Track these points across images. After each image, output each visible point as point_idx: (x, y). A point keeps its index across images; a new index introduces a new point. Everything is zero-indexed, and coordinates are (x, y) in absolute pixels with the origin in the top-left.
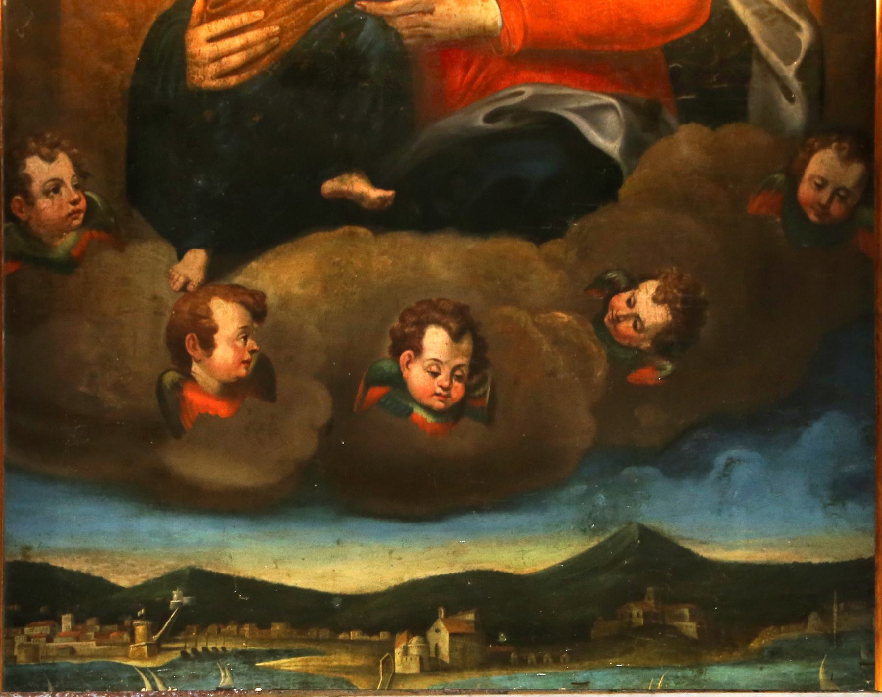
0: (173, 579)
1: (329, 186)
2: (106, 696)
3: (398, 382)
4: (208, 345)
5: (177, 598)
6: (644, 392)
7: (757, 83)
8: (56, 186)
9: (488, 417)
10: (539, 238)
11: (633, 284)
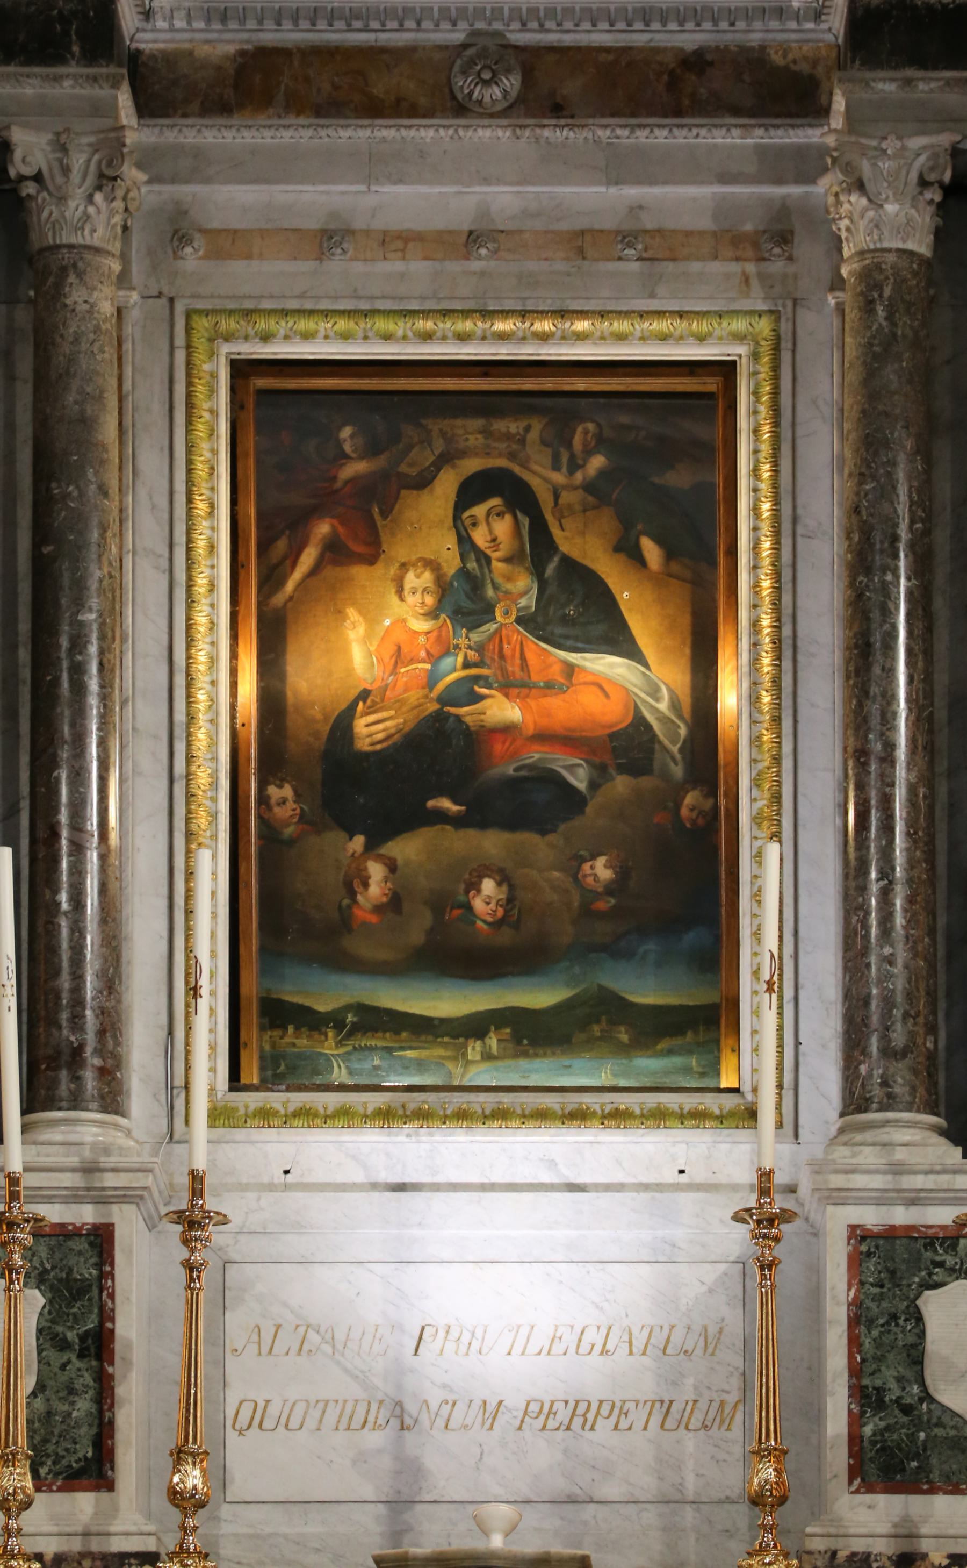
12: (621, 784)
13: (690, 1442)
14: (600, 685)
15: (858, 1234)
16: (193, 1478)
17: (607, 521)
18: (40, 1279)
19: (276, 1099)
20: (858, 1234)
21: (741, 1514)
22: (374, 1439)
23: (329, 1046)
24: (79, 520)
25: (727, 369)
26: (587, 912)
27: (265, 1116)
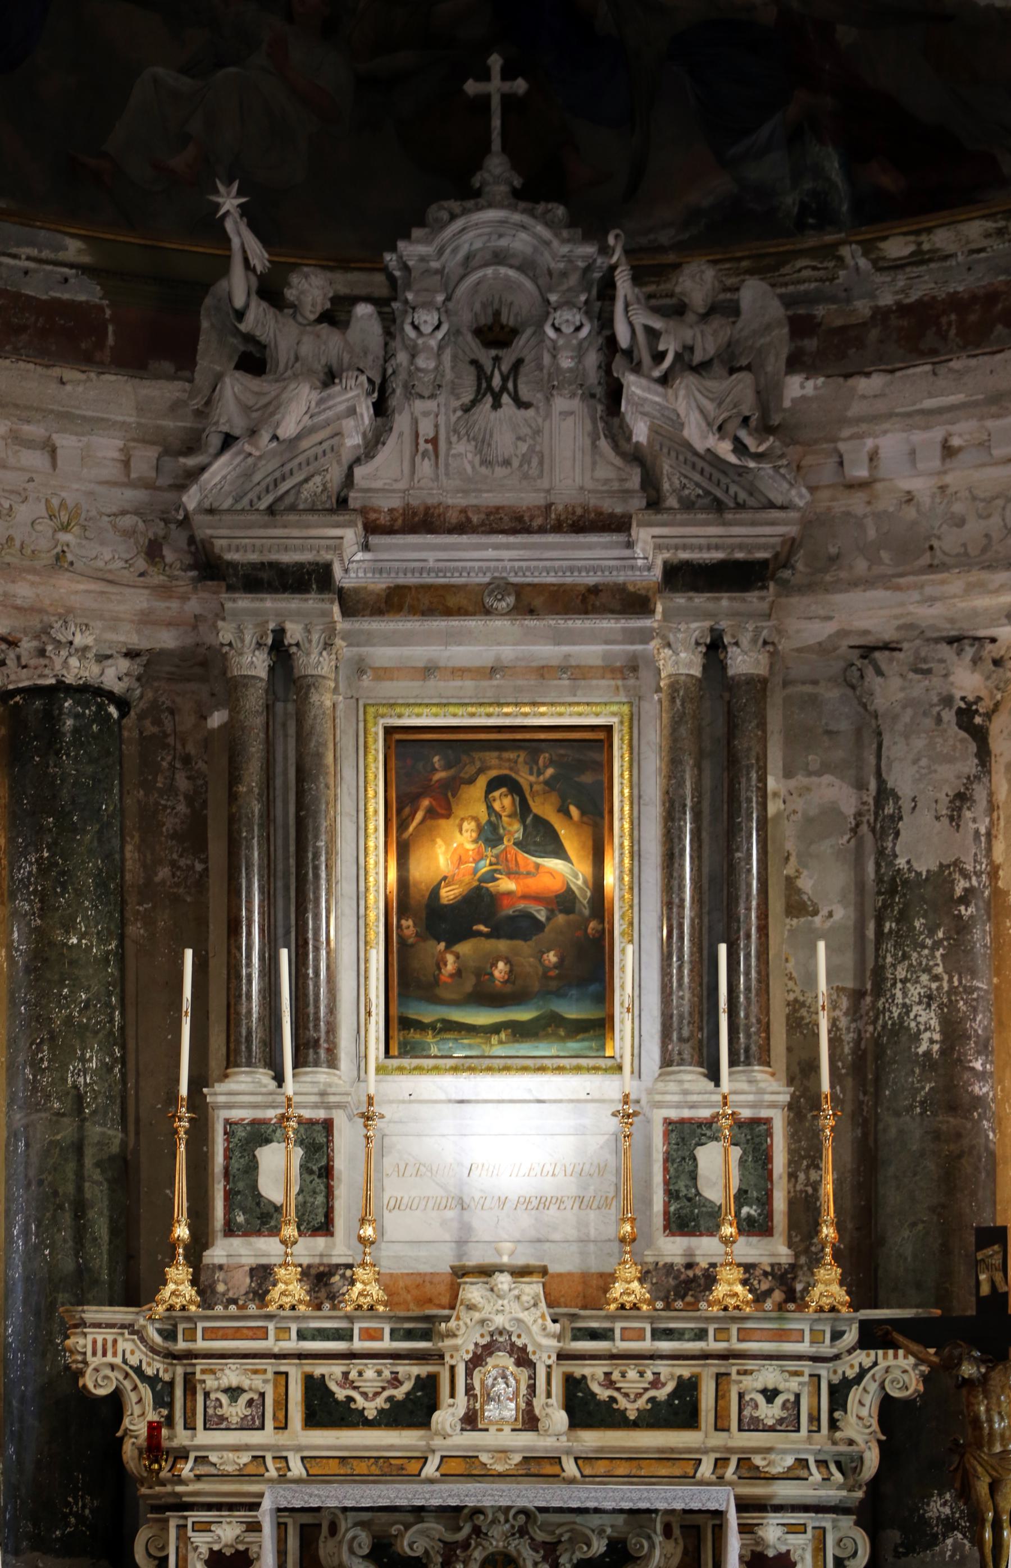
0: (438, 1021)
1: (475, 928)
2: (994, 1357)
3: (492, 975)
4: (446, 965)
5: (439, 1025)
6: (552, 978)
7: (577, 905)
8: (408, 927)
9: (514, 983)
10: (526, 940)
11: (548, 951)
12: (561, 918)
13: (592, 1215)
14: (551, 873)
15: (668, 1122)
16: (368, 1231)
17: (554, 798)
18: (300, 1142)
19: (406, 1062)
20: (668, 1122)
21: (616, 1246)
22: (450, 1214)
23: (429, 1038)
24: (317, 800)
25: (608, 729)
26: (545, 976)
27: (401, 1069)
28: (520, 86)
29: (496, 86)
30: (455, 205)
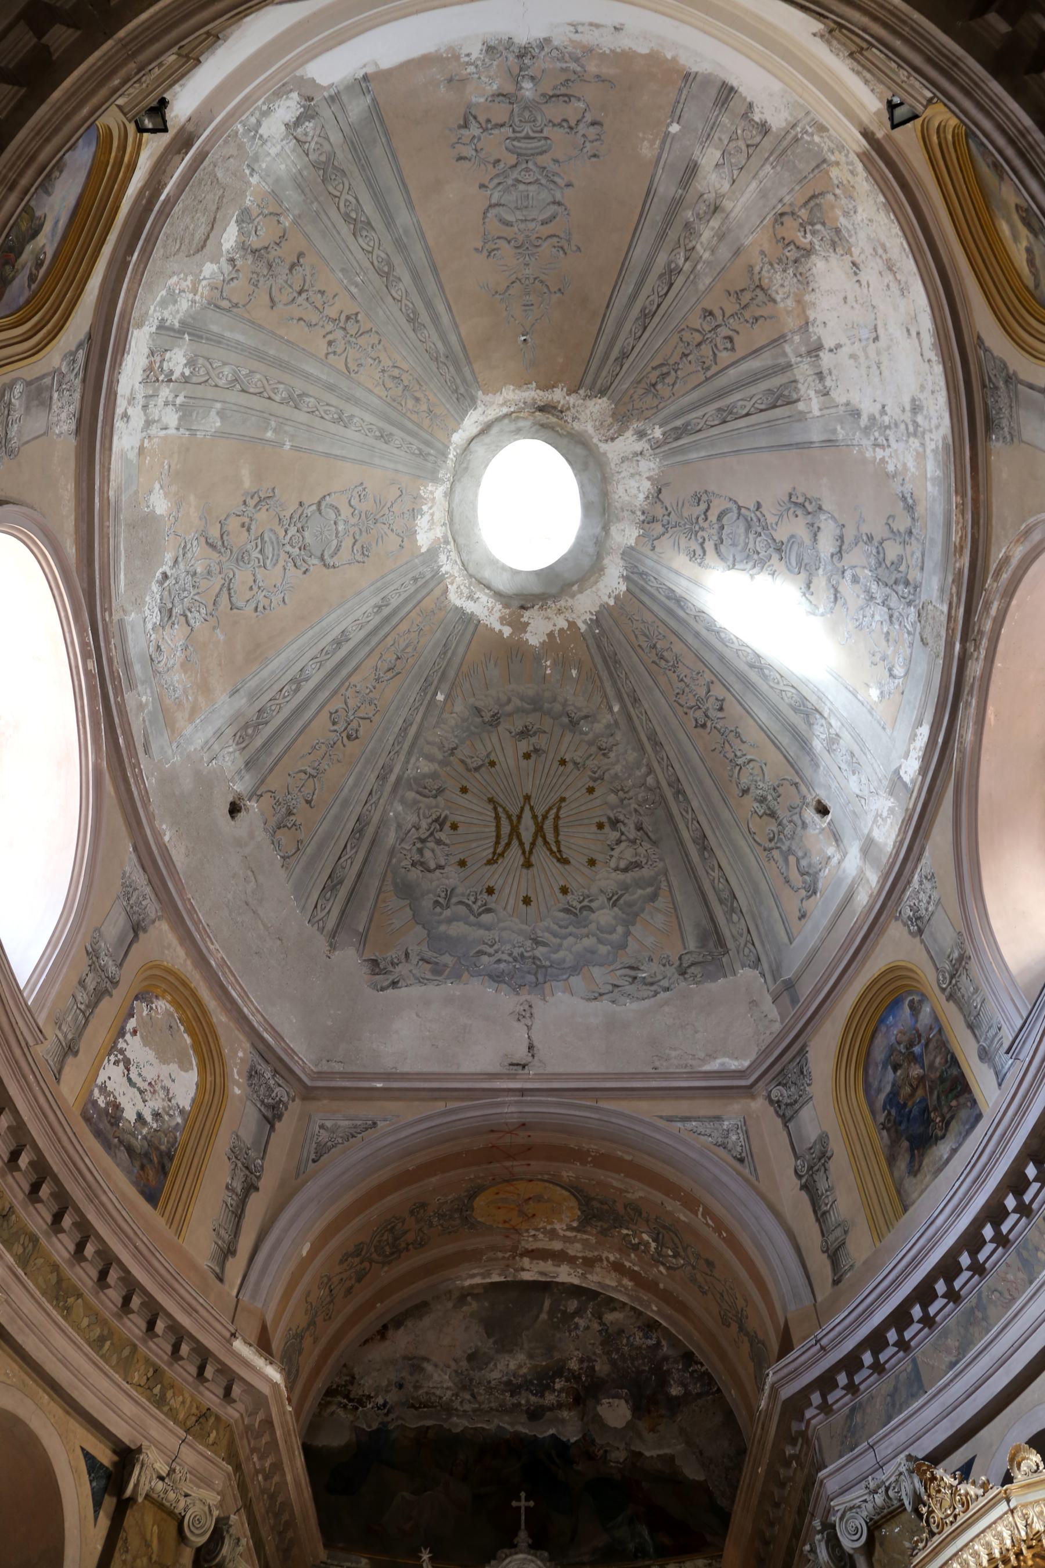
28: (532, 1504)
29: (523, 1504)
30: (507, 1551)
